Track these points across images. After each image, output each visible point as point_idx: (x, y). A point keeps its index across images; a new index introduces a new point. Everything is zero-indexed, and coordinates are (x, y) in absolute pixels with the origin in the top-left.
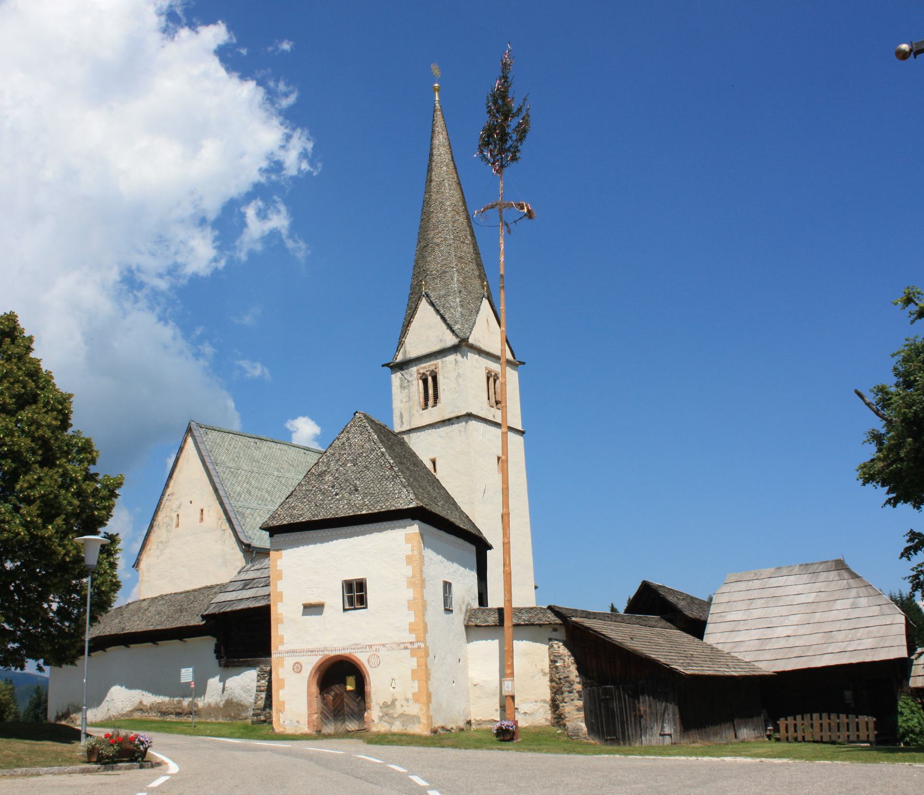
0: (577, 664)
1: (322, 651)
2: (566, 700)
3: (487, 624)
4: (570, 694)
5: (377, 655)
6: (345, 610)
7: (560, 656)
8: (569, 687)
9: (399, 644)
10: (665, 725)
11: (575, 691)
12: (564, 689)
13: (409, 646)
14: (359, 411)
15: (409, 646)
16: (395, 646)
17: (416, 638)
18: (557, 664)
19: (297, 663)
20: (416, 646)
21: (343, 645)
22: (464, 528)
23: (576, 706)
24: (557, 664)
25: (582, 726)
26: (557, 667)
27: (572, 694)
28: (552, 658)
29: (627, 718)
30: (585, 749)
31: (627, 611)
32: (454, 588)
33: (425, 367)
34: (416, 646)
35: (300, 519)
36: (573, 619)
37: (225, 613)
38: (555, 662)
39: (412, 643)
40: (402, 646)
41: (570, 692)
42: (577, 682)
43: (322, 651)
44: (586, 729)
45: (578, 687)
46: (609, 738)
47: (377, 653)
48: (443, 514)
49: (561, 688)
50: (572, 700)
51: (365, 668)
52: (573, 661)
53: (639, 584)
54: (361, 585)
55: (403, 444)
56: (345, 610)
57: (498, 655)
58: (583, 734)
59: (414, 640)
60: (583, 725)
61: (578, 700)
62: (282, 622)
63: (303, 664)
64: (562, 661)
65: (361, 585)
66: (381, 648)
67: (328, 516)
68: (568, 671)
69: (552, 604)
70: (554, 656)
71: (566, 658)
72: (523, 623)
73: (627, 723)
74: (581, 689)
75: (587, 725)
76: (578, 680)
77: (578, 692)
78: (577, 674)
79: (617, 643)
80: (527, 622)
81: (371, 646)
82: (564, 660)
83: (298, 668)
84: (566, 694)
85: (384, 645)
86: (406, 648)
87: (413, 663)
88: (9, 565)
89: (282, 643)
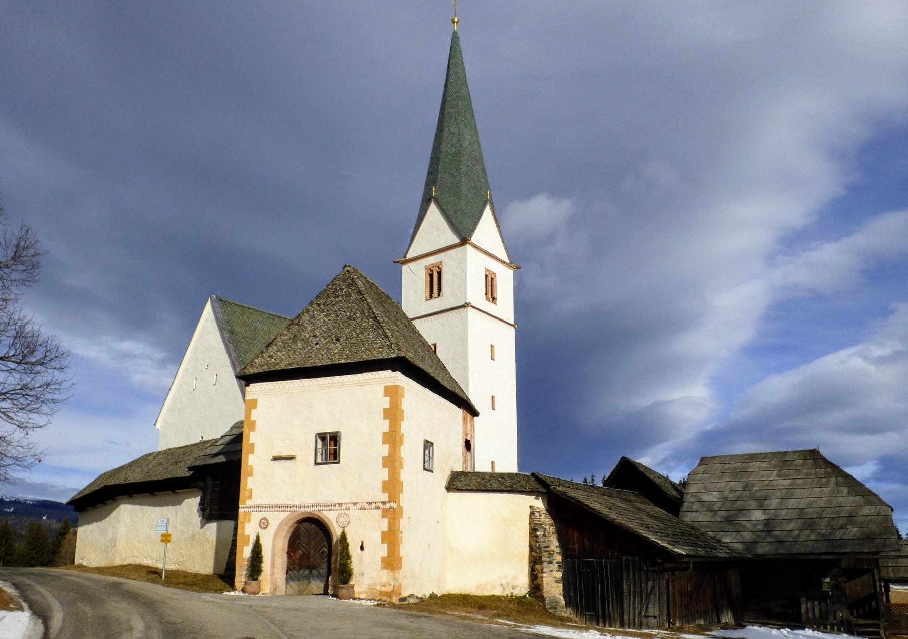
0: (558, 534)
1: (290, 507)
2: (545, 570)
3: (468, 487)
4: (550, 565)
5: (347, 514)
6: (316, 464)
7: (541, 525)
8: (549, 557)
9: (370, 503)
10: (650, 606)
11: (555, 562)
12: (544, 559)
13: (381, 506)
14: (347, 265)
15: (381, 506)
16: (366, 506)
17: (389, 497)
18: (538, 533)
19: (263, 519)
20: (388, 506)
21: (317, 502)
22: (451, 389)
23: (555, 578)
24: (538, 533)
25: (560, 599)
26: (537, 536)
27: (552, 565)
28: (533, 526)
29: (608, 596)
30: (563, 622)
31: (607, 482)
32: (437, 450)
33: (432, 260)
34: (388, 506)
35: (277, 367)
36: (558, 488)
37: (208, 465)
38: (536, 530)
39: (384, 503)
40: (374, 506)
41: (550, 563)
42: (557, 553)
43: (290, 507)
44: (564, 602)
45: (559, 558)
46: (587, 613)
47: (347, 512)
48: (430, 371)
49: (540, 558)
50: (551, 571)
51: (334, 527)
52: (554, 531)
53: (619, 459)
54: (335, 438)
55: (414, 331)
56: (316, 464)
57: (241, 483)
58: (561, 607)
59: (387, 500)
60: (562, 598)
61: (557, 571)
62: (252, 475)
63: (269, 520)
64: (543, 530)
65: (335, 438)
66: (351, 506)
67: (306, 364)
68: (548, 541)
69: (535, 472)
70: (535, 524)
71: (547, 527)
72: (505, 489)
73: (608, 601)
74: (561, 561)
75: (565, 598)
76: (558, 550)
77: (558, 563)
78: (558, 544)
79: (602, 516)
80: (509, 489)
81: (340, 504)
82: (545, 529)
83: (264, 524)
84: (545, 564)
85: (355, 504)
86: (378, 508)
87: (385, 525)
88: (831, 594)
89: (250, 497)
